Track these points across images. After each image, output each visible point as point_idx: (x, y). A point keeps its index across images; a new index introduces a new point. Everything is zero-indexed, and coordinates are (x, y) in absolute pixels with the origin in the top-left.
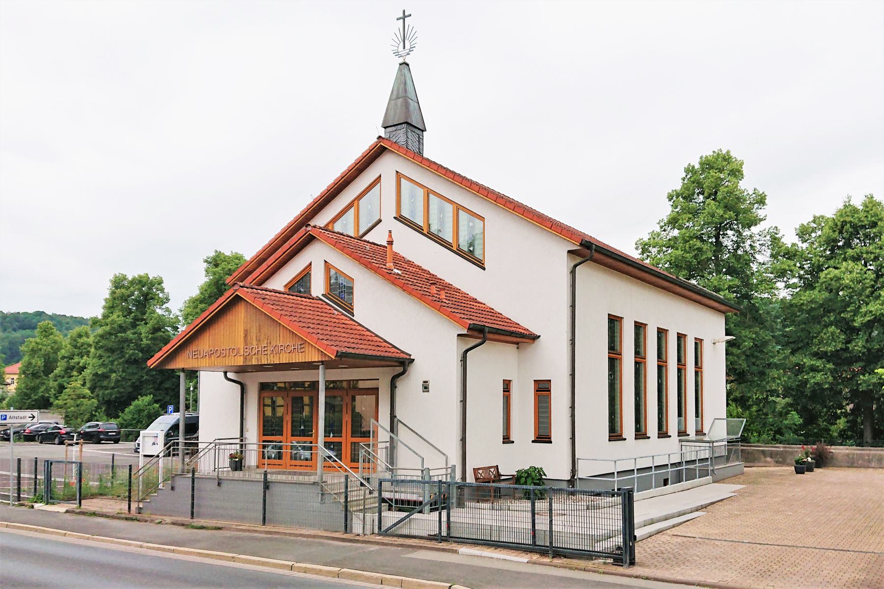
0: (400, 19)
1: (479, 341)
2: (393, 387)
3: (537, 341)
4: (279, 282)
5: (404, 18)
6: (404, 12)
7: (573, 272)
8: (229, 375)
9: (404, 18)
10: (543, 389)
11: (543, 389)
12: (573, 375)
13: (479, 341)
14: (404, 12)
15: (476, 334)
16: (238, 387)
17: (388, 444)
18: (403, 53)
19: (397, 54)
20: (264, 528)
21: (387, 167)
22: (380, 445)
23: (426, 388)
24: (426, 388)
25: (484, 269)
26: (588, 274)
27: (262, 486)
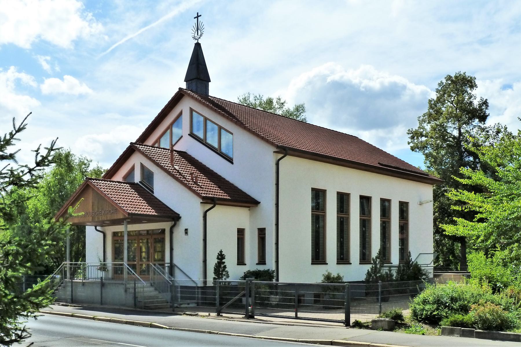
0: (195, 18)
1: (212, 205)
2: (171, 233)
3: (259, 205)
4: (119, 177)
5: (198, 17)
6: (198, 13)
7: (277, 164)
8: (98, 228)
9: (198, 17)
10: (262, 232)
11: (262, 232)
12: (277, 225)
13: (212, 205)
14: (198, 13)
15: (209, 201)
16: (101, 235)
17: (169, 265)
18: (197, 37)
19: (194, 38)
20: (102, 306)
21: (185, 106)
22: (166, 265)
23: (186, 231)
24: (186, 231)
25: (232, 163)
26: (289, 163)
27: (99, 286)
